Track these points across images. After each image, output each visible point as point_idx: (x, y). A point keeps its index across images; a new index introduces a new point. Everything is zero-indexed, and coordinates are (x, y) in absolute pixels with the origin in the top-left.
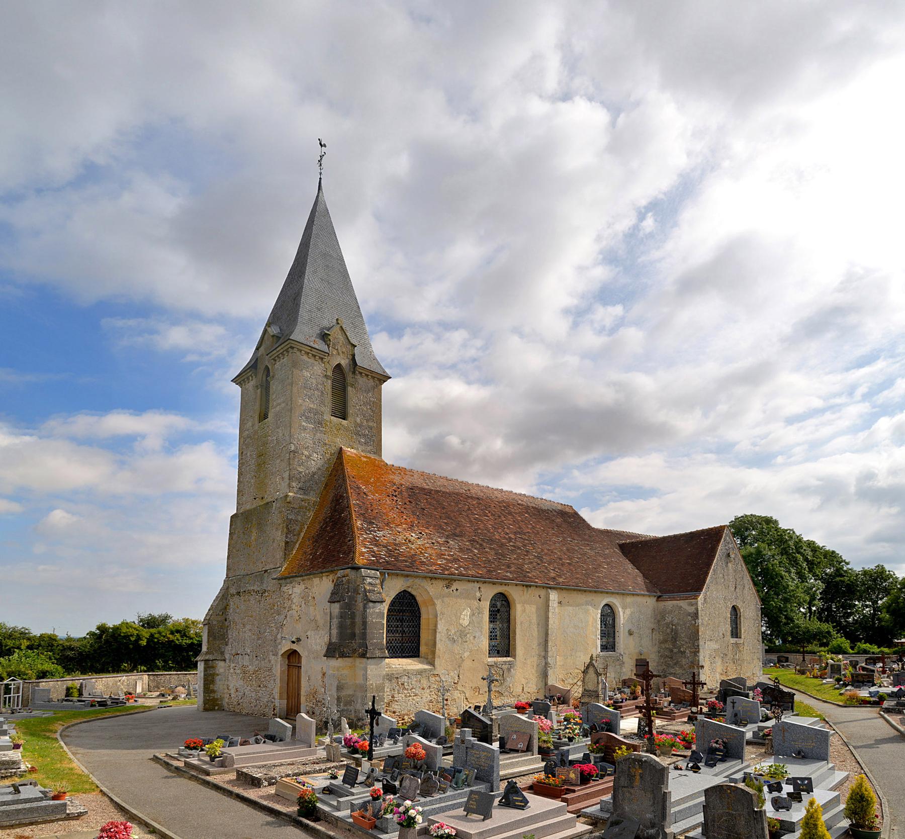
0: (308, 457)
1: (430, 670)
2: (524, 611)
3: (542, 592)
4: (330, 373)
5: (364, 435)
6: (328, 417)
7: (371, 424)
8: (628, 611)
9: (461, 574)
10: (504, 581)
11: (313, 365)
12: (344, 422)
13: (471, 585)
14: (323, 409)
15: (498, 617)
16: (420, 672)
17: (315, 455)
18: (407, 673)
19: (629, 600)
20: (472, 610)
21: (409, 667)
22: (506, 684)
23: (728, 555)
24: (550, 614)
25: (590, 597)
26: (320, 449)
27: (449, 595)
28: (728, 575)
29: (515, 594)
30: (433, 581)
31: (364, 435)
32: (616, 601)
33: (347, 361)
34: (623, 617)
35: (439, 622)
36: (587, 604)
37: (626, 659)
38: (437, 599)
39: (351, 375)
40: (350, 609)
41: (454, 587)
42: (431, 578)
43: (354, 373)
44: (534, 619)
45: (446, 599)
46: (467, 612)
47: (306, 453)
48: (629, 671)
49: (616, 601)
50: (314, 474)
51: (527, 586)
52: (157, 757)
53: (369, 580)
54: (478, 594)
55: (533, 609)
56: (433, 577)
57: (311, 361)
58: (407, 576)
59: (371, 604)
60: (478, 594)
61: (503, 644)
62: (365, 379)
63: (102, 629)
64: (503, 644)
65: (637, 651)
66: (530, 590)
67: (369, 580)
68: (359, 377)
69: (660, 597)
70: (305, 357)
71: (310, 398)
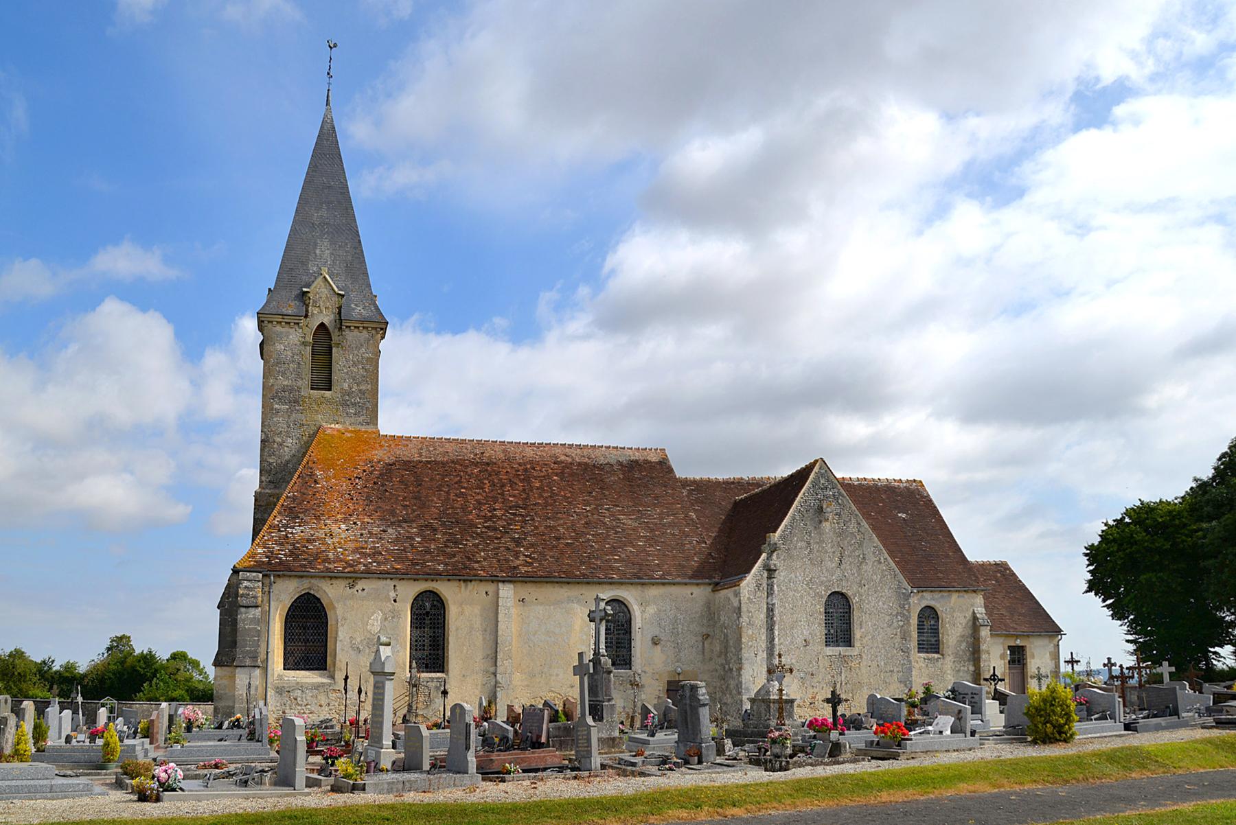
0: (281, 445)
1: (330, 685)
2: (462, 613)
3: (491, 587)
4: (310, 339)
5: (354, 404)
6: (307, 392)
7: (363, 387)
8: (651, 610)
9: (368, 572)
10: (435, 575)
11: (287, 335)
12: (328, 393)
13: (381, 583)
14: (300, 383)
15: (427, 622)
16: (317, 687)
17: (290, 440)
18: (301, 687)
19: (654, 592)
20: (384, 614)
21: (304, 680)
22: (433, 706)
23: (820, 510)
24: (500, 616)
25: (563, 592)
26: (295, 433)
27: (352, 597)
28: (821, 542)
29: (448, 591)
30: (334, 581)
31: (354, 404)
32: (629, 595)
33: (332, 317)
34: (642, 617)
35: (340, 629)
36: (570, 600)
37: (645, 680)
38: (338, 601)
39: (337, 333)
40: (230, 616)
41: (359, 586)
42: (331, 578)
43: (340, 329)
44: (478, 623)
45: (349, 602)
46: (379, 615)
47: (278, 440)
48: (652, 695)
49: (629, 595)
50: (288, 462)
51: (465, 581)
52: (718, 751)
53: (246, 583)
54: (392, 594)
55: (477, 610)
56: (331, 576)
57: (287, 329)
58: (302, 577)
59: (243, 610)
60: (392, 594)
61: (431, 651)
62: (356, 332)
63: (1094, 586)
64: (431, 651)
65: (670, 668)
66: (470, 586)
67: (246, 583)
68: (347, 332)
69: (717, 584)
70: (278, 328)
71: (283, 374)
